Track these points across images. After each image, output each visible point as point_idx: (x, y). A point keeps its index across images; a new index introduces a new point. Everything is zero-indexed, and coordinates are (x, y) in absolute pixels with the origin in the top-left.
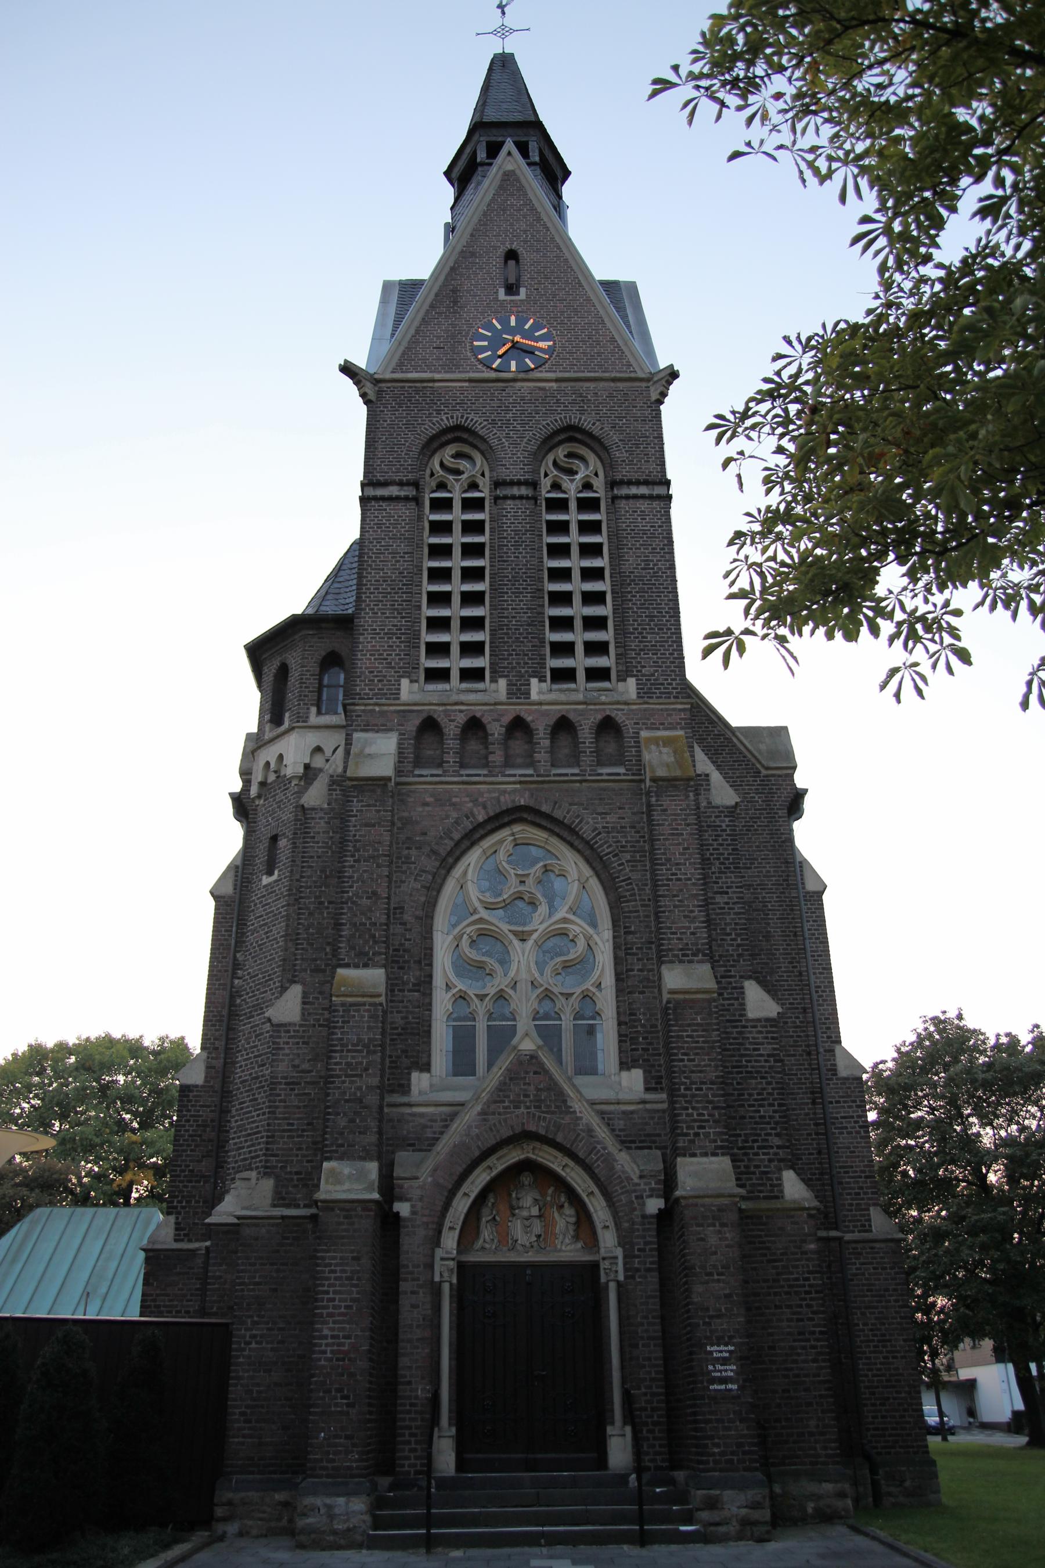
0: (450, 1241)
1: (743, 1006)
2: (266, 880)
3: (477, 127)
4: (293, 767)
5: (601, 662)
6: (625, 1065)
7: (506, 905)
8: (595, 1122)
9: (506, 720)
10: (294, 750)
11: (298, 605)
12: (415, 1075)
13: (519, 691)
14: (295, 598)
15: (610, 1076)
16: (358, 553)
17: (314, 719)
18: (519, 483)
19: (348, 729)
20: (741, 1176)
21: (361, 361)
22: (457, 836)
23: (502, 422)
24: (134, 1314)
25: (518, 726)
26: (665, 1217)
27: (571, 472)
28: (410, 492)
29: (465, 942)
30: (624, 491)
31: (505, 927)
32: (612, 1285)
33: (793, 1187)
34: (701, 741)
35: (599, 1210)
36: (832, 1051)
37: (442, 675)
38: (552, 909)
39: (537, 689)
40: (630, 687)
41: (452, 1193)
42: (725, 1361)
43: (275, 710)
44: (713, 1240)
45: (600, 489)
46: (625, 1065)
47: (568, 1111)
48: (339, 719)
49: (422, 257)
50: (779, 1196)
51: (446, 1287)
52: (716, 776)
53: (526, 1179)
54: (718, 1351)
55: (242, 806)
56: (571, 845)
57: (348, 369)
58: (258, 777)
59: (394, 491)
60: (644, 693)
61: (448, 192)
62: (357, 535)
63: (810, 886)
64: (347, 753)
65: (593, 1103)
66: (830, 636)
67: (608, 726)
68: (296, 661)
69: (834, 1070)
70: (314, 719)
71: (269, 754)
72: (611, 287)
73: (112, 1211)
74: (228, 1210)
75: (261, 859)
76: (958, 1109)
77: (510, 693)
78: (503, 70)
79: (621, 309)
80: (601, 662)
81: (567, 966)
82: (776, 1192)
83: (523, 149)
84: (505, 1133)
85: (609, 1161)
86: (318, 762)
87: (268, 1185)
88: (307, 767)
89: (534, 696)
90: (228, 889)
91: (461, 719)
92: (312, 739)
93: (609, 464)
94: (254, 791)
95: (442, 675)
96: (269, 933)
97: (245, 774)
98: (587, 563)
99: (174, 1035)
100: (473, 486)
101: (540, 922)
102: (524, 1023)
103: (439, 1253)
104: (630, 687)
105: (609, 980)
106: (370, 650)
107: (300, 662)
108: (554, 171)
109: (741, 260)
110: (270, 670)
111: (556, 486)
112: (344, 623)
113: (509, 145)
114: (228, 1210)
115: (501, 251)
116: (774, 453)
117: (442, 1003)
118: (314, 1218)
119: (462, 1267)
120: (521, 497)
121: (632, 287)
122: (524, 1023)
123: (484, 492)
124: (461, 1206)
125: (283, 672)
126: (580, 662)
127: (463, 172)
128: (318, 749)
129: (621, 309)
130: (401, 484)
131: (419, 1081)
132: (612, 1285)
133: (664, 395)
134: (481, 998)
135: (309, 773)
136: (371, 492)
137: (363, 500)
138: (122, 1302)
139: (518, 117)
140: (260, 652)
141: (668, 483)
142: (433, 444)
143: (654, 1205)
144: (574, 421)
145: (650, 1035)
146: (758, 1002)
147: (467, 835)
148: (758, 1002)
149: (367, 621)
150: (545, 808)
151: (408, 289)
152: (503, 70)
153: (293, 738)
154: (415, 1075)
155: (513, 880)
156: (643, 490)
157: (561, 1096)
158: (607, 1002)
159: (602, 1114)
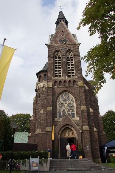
0: (59, 135)
1: (89, 110)
3: (58, 19)
4: (41, 86)
5: (73, 74)
6: (77, 117)
7: (64, 100)
8: (74, 123)
9: (64, 81)
10: (41, 84)
11: (41, 69)
12: (55, 118)
13: (65, 78)
14: (41, 69)
16: (47, 63)
17: (43, 81)
19: (47, 82)
20: (90, 128)
21: (47, 44)
23: (62, 49)
24: (27, 142)
25: (65, 81)
26: (82, 133)
27: (70, 54)
28: (53, 57)
29: (60, 104)
30: (75, 56)
31: (64, 103)
33: (95, 129)
34: (85, 83)
35: (75, 132)
36: (99, 115)
37: (57, 76)
38: (69, 100)
39: (67, 77)
40: (77, 77)
41: (60, 130)
42: (88, 147)
43: (39, 81)
46: (77, 117)
47: (71, 122)
48: (46, 81)
49: (53, 32)
50: (93, 130)
51: (59, 140)
52: (86, 86)
54: (88, 146)
55: (36, 90)
56: (71, 94)
57: (46, 44)
58: (38, 88)
59: (51, 57)
60: (78, 77)
61: (56, 25)
62: (47, 61)
63: (96, 97)
64: (47, 85)
65: (74, 121)
66: (98, 44)
67: (74, 81)
68: (41, 75)
69: (99, 117)
70: (43, 81)
71: (39, 85)
72: (73, 35)
73: (23, 132)
74: (36, 132)
75: (38, 96)
77: (64, 78)
78: (61, 12)
79: (74, 37)
80: (73, 74)
82: (93, 130)
83: (63, 21)
84: (65, 124)
86: (44, 86)
87: (40, 130)
88: (43, 86)
89: (67, 78)
90: (35, 99)
92: (44, 83)
93: (74, 53)
94: (37, 89)
95: (57, 76)
96: (40, 102)
97: (36, 87)
98: (72, 72)
99: (28, 113)
100: (59, 56)
101: (68, 102)
102: (66, 113)
103: (58, 137)
104: (77, 77)
105: (75, 108)
106: (49, 74)
107: (42, 75)
108: (67, 23)
109: (88, 40)
110: (39, 76)
111: (68, 56)
112: (46, 71)
113: (62, 20)
114: (36, 132)
116: (91, 35)
117: (58, 111)
118: (45, 133)
119: (61, 138)
121: (75, 34)
122: (66, 113)
124: (60, 132)
125: (40, 76)
126: (71, 74)
127: (57, 23)
128: (44, 84)
129: (74, 37)
130: (52, 56)
131: (56, 119)
133: (79, 46)
134: (62, 110)
135: (43, 87)
136: (49, 57)
137: (48, 58)
138: (26, 141)
139: (63, 17)
140: (37, 74)
141: (80, 55)
142: (55, 52)
143: (81, 131)
145: (81, 114)
146: (91, 110)
147: (60, 93)
148: (91, 110)
150: (68, 90)
151: (52, 35)
152: (61, 12)
153: (41, 83)
154: (55, 118)
155: (65, 98)
156: (77, 56)
157: (71, 120)
158: (75, 110)
159: (75, 122)
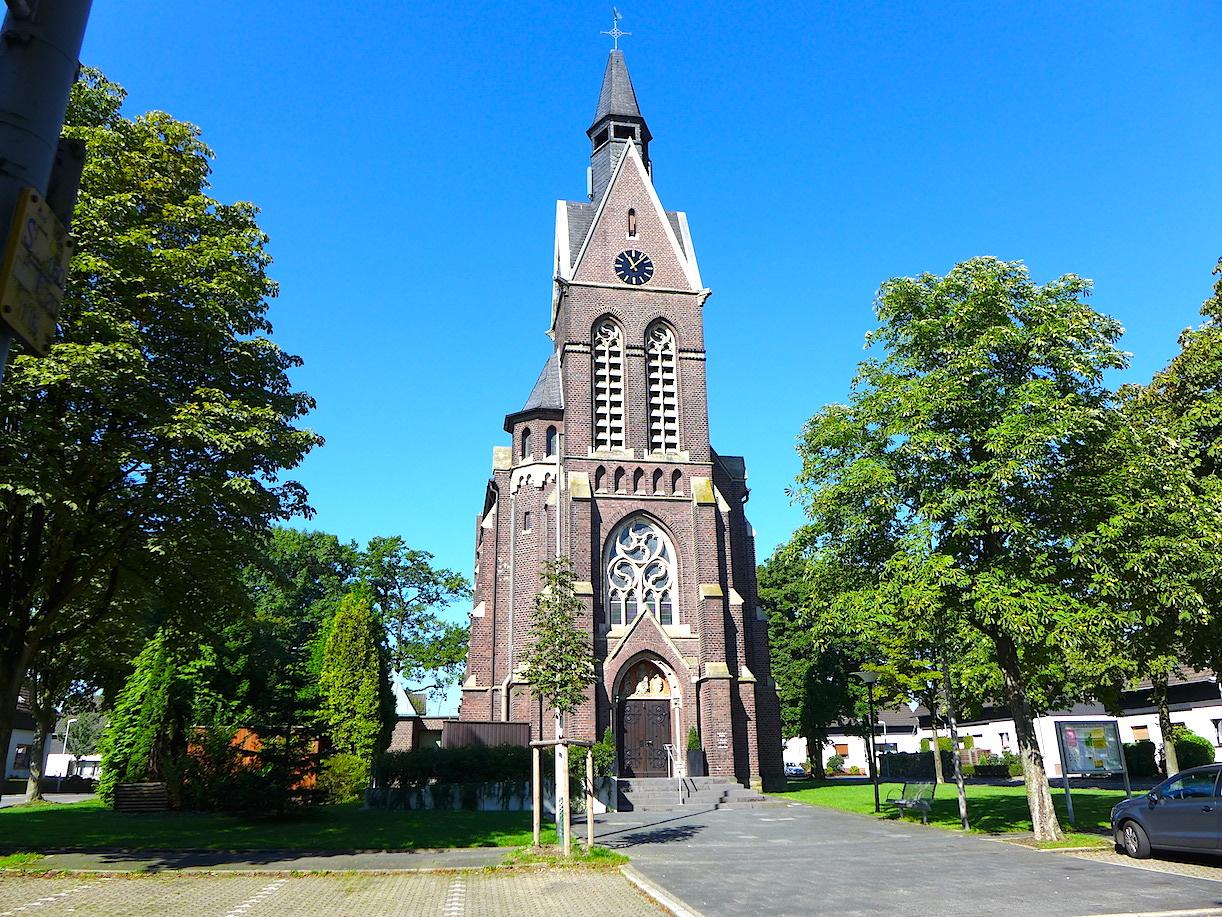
2: (524, 532)
15: (474, 619)
18: (637, 348)
22: (615, 522)
32: (677, 710)
44: (720, 694)
45: (672, 351)
53: (642, 666)
76: (29, 761)
81: (657, 579)
85: (678, 661)
91: (615, 467)
93: (679, 339)
115: (627, 209)
120: (639, 356)
123: (620, 348)
132: (677, 710)
144: (662, 315)
149: (570, 414)
155: (635, 541)
156: (693, 355)
